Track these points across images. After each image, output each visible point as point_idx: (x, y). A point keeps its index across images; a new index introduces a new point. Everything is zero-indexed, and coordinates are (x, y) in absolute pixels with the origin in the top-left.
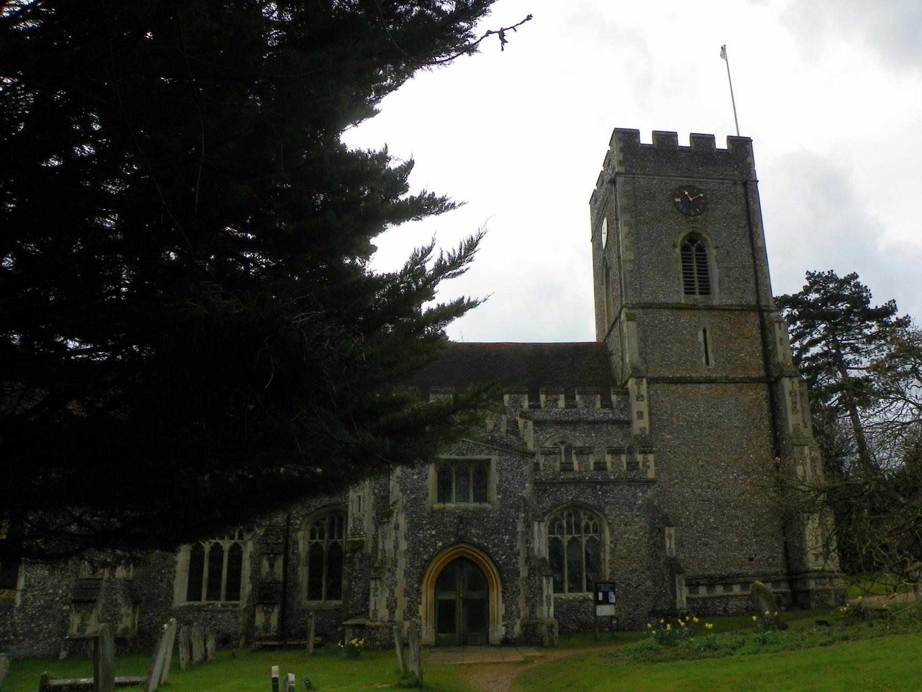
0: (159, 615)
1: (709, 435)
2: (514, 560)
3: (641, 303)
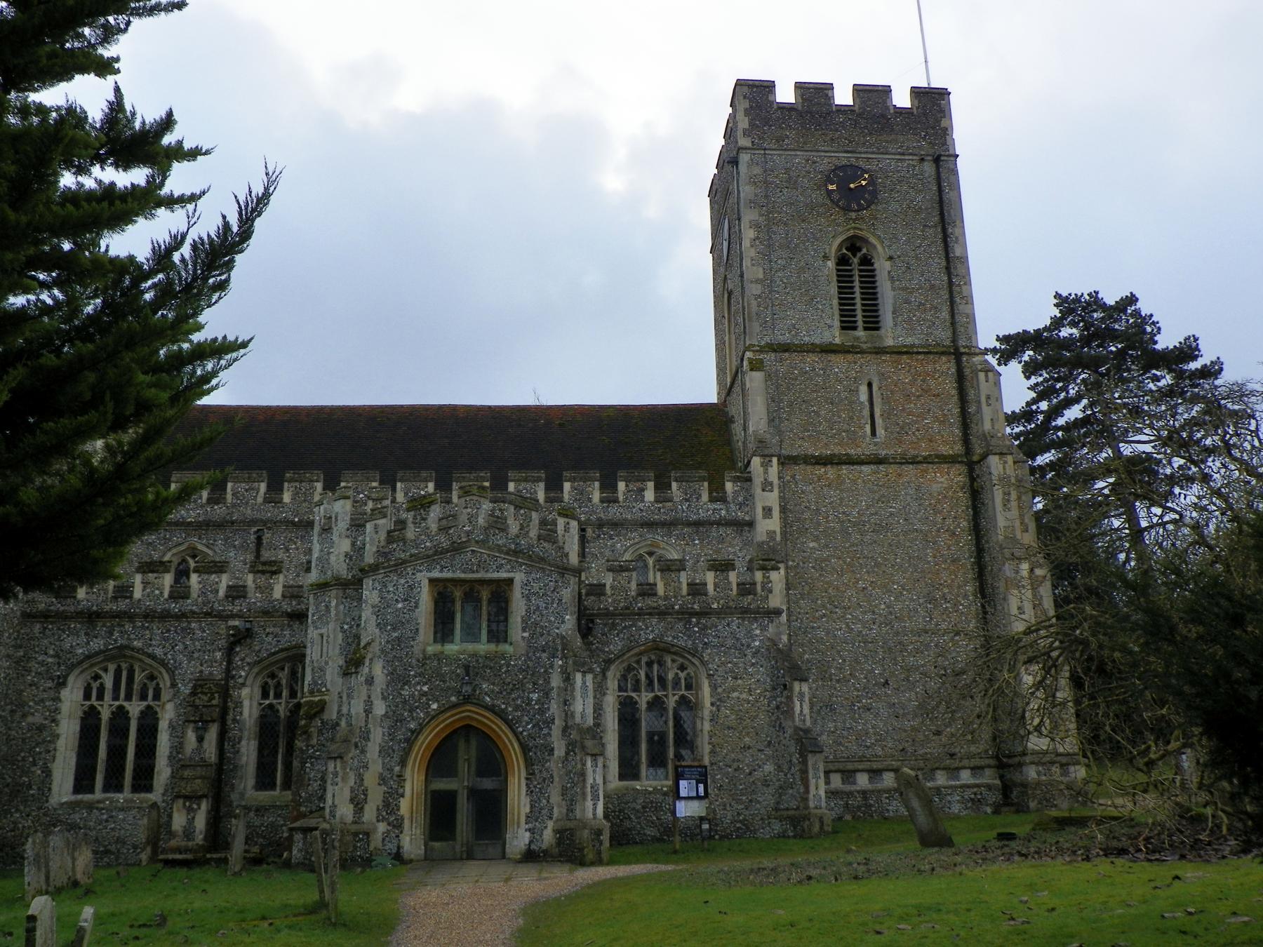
0: (28, 816)
1: (875, 542)
2: (545, 731)
3: (772, 344)
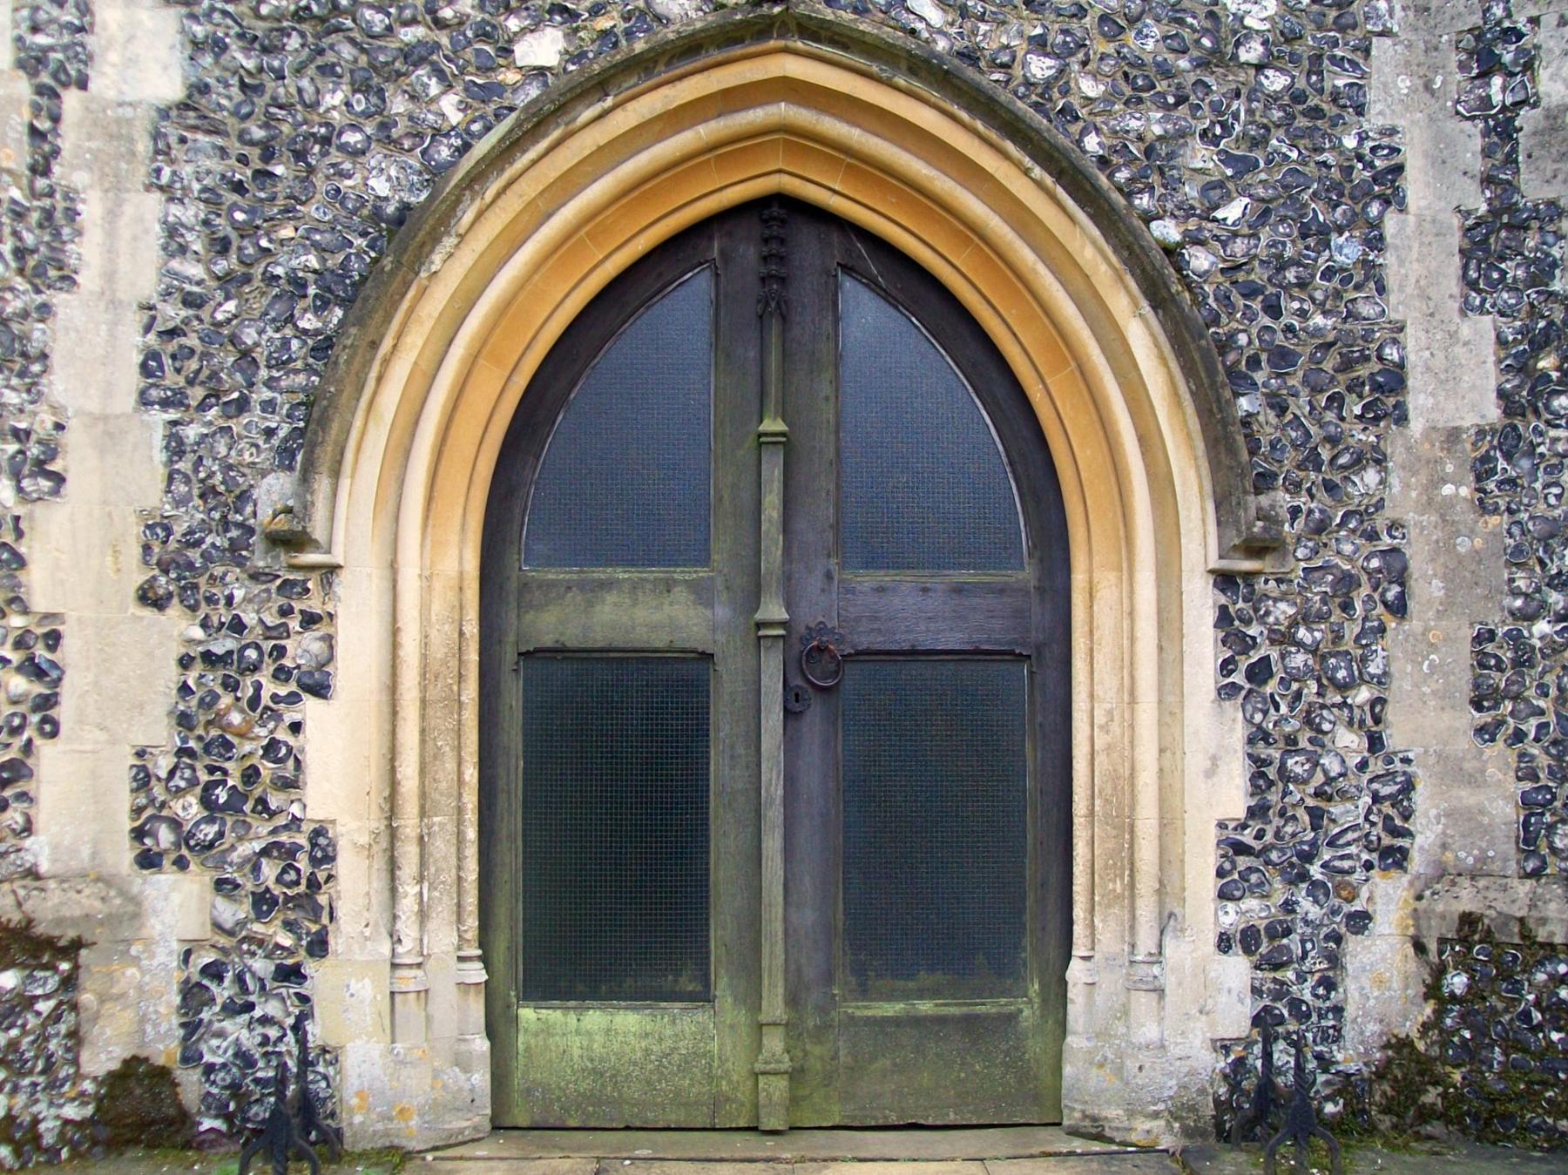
2: (1347, 250)
